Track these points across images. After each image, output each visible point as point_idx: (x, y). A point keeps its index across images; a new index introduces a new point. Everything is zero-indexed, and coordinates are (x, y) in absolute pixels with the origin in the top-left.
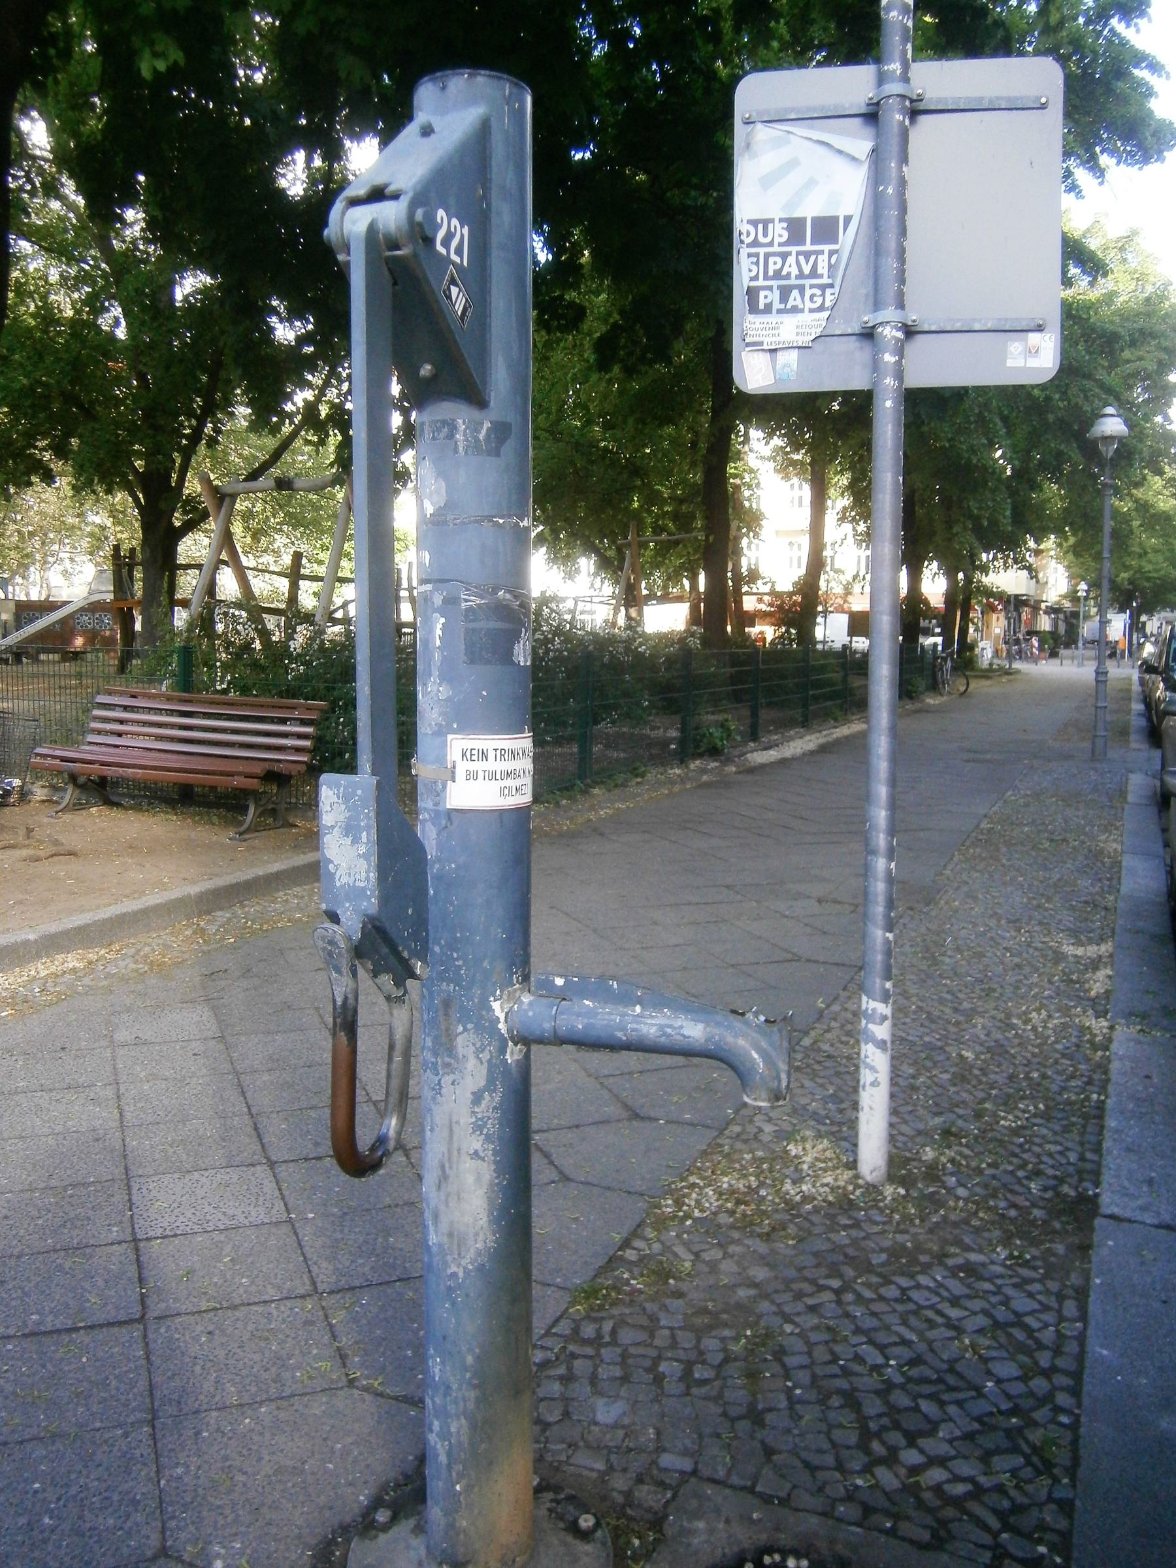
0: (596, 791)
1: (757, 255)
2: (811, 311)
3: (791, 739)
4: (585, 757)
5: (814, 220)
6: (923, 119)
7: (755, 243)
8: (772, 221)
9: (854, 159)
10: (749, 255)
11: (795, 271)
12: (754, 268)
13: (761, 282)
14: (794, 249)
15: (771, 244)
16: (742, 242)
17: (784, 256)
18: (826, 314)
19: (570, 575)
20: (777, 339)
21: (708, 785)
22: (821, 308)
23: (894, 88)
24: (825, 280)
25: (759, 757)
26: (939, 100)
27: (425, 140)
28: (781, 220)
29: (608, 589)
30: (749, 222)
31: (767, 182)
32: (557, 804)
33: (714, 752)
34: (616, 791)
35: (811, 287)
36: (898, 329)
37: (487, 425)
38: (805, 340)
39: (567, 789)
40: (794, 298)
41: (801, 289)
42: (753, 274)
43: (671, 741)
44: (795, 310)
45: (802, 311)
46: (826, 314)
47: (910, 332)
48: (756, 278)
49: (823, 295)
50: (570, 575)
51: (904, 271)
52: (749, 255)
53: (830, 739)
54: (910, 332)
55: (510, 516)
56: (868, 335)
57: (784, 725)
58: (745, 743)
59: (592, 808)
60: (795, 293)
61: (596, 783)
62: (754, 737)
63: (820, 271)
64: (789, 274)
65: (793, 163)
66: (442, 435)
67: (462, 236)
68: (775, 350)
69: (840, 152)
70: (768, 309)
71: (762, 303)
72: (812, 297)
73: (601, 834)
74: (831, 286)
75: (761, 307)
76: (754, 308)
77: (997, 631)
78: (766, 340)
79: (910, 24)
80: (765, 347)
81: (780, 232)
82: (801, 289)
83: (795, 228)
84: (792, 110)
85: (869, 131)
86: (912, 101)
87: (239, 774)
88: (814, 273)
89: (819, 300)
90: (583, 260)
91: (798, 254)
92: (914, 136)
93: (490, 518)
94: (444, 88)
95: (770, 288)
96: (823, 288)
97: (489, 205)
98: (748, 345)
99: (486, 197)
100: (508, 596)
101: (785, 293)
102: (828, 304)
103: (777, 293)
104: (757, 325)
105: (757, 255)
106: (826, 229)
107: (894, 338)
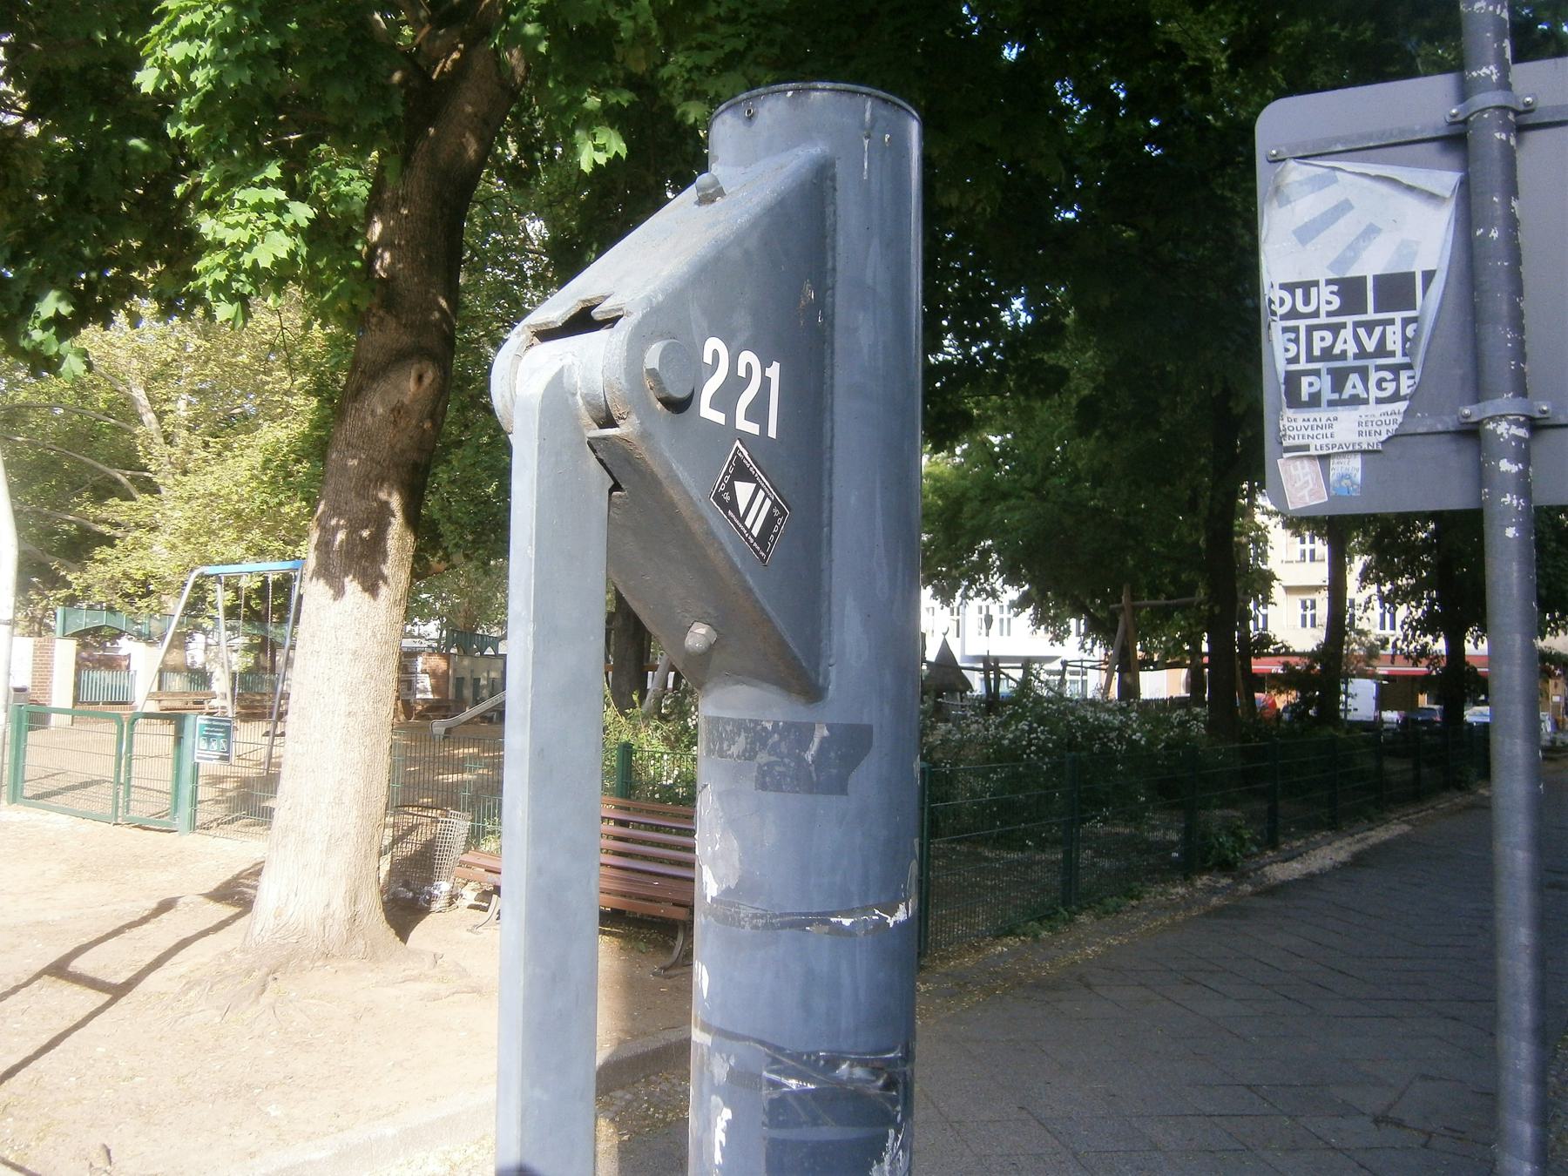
0: (1083, 918)
1: (1296, 330)
2: (1379, 401)
3: (1317, 846)
4: (1069, 868)
5: (1376, 278)
6: (1533, 137)
7: (1293, 314)
8: (1316, 284)
9: (1432, 196)
10: (1285, 330)
11: (1352, 349)
12: (1292, 347)
13: (1303, 365)
14: (1349, 320)
15: (1316, 314)
16: (1274, 313)
17: (1335, 329)
18: (1402, 406)
19: (1059, 638)
20: (1329, 441)
21: (1219, 912)
22: (1395, 397)
23: (1494, 98)
24: (1399, 359)
25: (1281, 872)
26: (1557, 109)
27: (704, 208)
28: (1329, 282)
29: (1099, 653)
30: (1283, 287)
31: (1305, 234)
32: (1036, 936)
33: (1226, 866)
34: (1108, 919)
35: (1379, 368)
36: (1519, 425)
37: (822, 732)
38: (1372, 442)
39: (1048, 917)
40: (1353, 384)
41: (1363, 373)
42: (1291, 354)
43: (1173, 844)
44: (1355, 401)
45: (1365, 402)
46: (1402, 406)
47: (1535, 426)
48: (1295, 360)
49: (1397, 379)
50: (1059, 638)
51: (1522, 343)
52: (1285, 330)
53: (1363, 846)
54: (1535, 426)
55: (866, 910)
56: (1471, 433)
57: (1310, 826)
58: (1262, 853)
59: (1077, 945)
60: (1354, 378)
61: (1082, 909)
62: (1274, 845)
63: (1390, 347)
64: (1344, 352)
65: (1344, 207)
66: (734, 750)
67: (766, 382)
68: (1328, 456)
69: (1410, 189)
70: (1315, 401)
71: (1305, 392)
72: (1380, 382)
73: (1088, 986)
74: (1409, 367)
75: (1305, 397)
76: (1294, 401)
77: (1556, 699)
78: (1313, 443)
79: (1505, 15)
80: (1312, 452)
81: (1327, 299)
82: (1363, 373)
83: (1351, 292)
84: (1337, 140)
85: (1452, 159)
86: (1517, 113)
87: (666, 900)
88: (1381, 350)
89: (1390, 388)
90: (1067, 321)
91: (1357, 325)
92: (1522, 158)
93: (823, 918)
94: (751, 118)
95: (1317, 373)
96: (1396, 370)
97: (830, 320)
98: (1288, 450)
99: (819, 304)
100: (859, 1072)
101: (1339, 379)
102: (1404, 391)
103: (1327, 380)
104: (1300, 423)
105: (1296, 330)
106: (1397, 290)
107: (1515, 437)
